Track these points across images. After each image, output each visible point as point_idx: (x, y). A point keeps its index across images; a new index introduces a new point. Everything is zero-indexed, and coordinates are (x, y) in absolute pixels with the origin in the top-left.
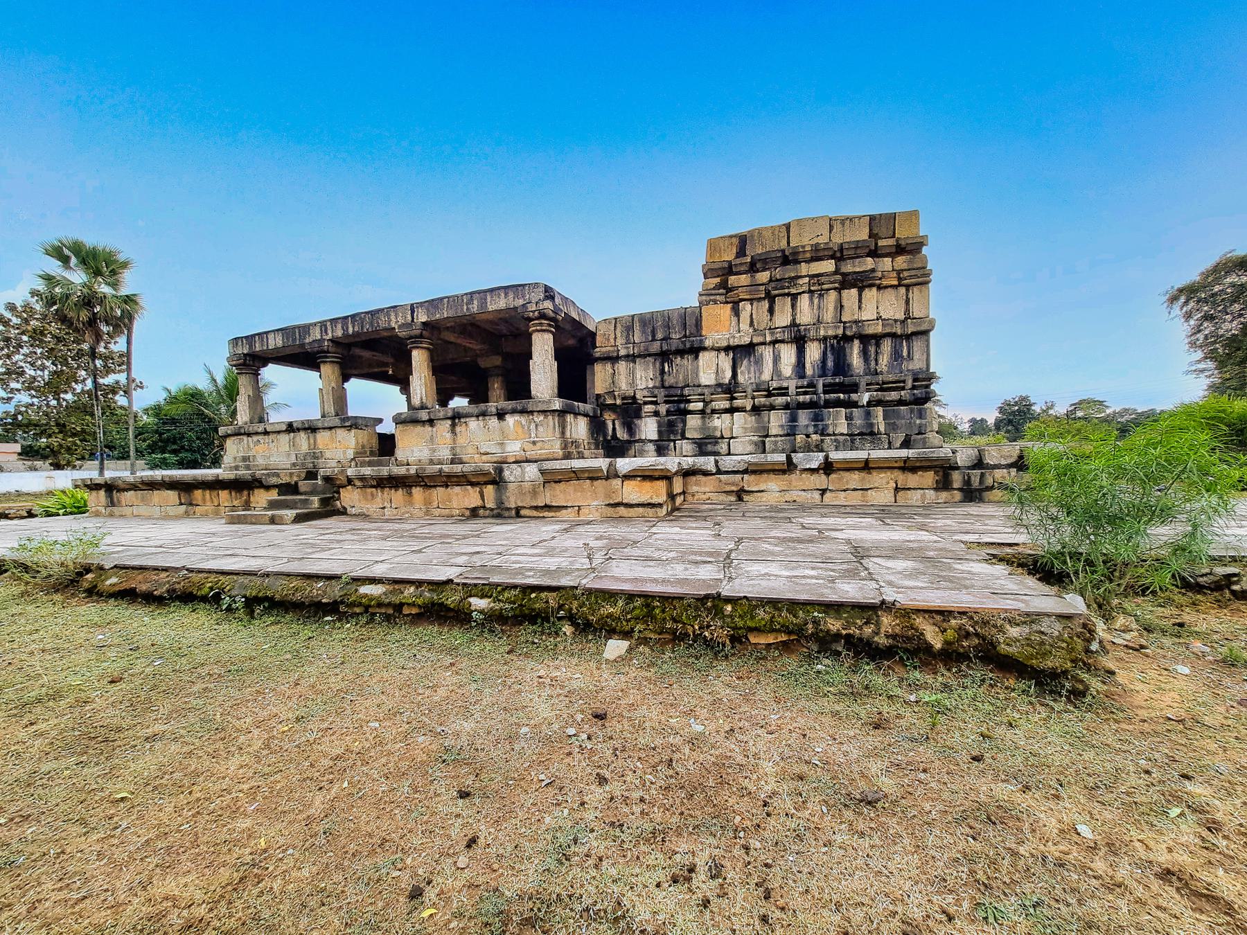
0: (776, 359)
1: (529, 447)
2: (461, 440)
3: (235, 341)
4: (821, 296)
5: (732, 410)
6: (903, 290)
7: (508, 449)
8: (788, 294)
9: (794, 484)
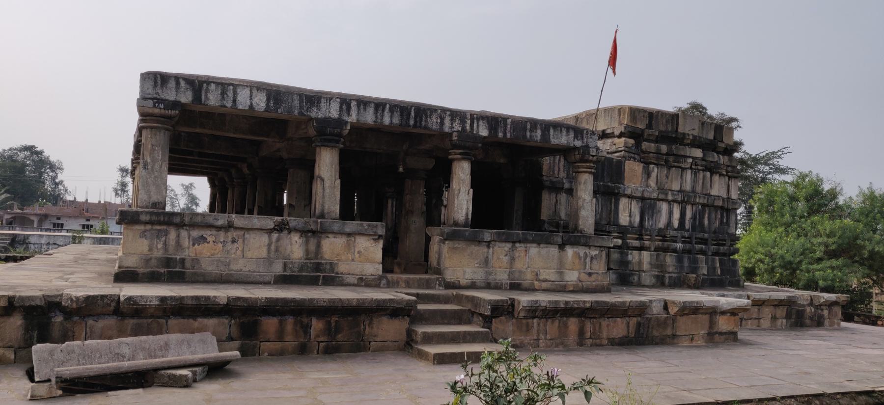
0: (671, 214)
1: (584, 277)
2: (519, 265)
3: (156, 80)
5: (641, 249)
6: (727, 178)
7: (567, 278)
8: (680, 167)
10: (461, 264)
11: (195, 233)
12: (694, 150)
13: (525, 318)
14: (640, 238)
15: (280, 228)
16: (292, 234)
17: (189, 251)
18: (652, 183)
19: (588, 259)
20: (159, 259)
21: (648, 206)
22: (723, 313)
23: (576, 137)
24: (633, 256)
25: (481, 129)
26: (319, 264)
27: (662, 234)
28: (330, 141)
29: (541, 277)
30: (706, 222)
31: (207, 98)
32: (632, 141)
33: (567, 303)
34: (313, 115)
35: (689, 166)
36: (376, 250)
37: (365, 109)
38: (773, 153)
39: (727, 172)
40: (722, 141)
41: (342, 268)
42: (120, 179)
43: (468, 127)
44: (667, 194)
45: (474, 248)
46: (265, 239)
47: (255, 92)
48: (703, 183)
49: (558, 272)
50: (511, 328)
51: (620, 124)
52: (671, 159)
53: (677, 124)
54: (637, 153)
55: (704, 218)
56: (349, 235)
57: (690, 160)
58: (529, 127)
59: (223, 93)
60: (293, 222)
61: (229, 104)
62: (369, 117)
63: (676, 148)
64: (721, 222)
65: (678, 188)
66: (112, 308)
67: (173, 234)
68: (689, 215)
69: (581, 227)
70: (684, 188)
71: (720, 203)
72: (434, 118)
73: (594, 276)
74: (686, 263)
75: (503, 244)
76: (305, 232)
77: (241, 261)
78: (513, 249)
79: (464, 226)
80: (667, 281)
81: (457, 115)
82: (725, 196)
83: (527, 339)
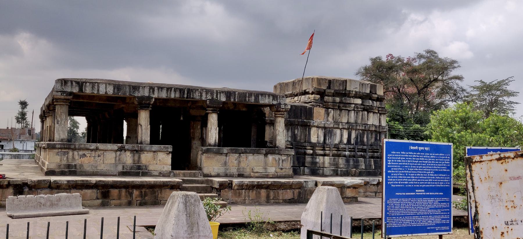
0: (342, 136)
2: (242, 165)
3: (64, 82)
4: (357, 113)
5: (324, 155)
6: (379, 114)
9: (368, 189)
10: (212, 165)
11: (81, 153)
12: (356, 99)
13: (238, 189)
14: (324, 150)
15: (121, 149)
16: (127, 152)
17: (78, 161)
18: (330, 119)
19: (281, 161)
20: (64, 165)
21: (328, 132)
22: (349, 187)
23: (273, 99)
24: (319, 160)
25: (222, 97)
26: (139, 166)
27: (337, 147)
28: (145, 107)
29: (255, 171)
30: (365, 139)
31: (85, 90)
32: (318, 96)
33: (258, 182)
34: (136, 95)
35: (353, 109)
36: (168, 159)
37: (162, 91)
38: (503, 81)
39: (379, 111)
40: (376, 94)
41: (151, 168)
42: (21, 110)
43: (215, 97)
44: (339, 125)
45: (219, 157)
46: (113, 154)
47: (108, 85)
48: (362, 118)
49: (264, 168)
50: (231, 195)
51: (312, 87)
52: (341, 105)
53: (346, 85)
54: (322, 103)
55: (364, 137)
56: (154, 152)
57: (353, 105)
58: (247, 95)
59: (93, 87)
60: (127, 146)
61: (96, 92)
62: (164, 95)
63: (345, 99)
64: (376, 139)
65: (346, 121)
66: (48, 185)
67: (71, 153)
68: (353, 135)
69: (277, 145)
70: (350, 121)
71: (374, 129)
72: (197, 93)
73: (284, 170)
74: (351, 163)
75: (234, 155)
76: (133, 151)
77: (103, 165)
78: (240, 157)
79: (214, 146)
80: (339, 172)
81: (209, 91)
82: (378, 124)
83: (239, 200)
